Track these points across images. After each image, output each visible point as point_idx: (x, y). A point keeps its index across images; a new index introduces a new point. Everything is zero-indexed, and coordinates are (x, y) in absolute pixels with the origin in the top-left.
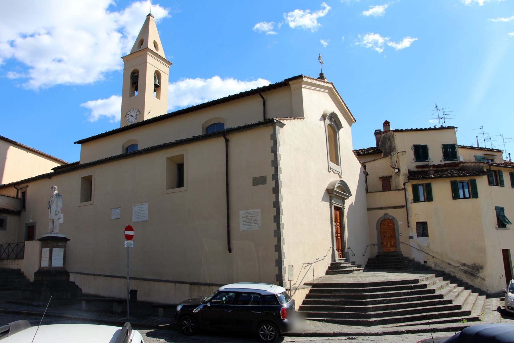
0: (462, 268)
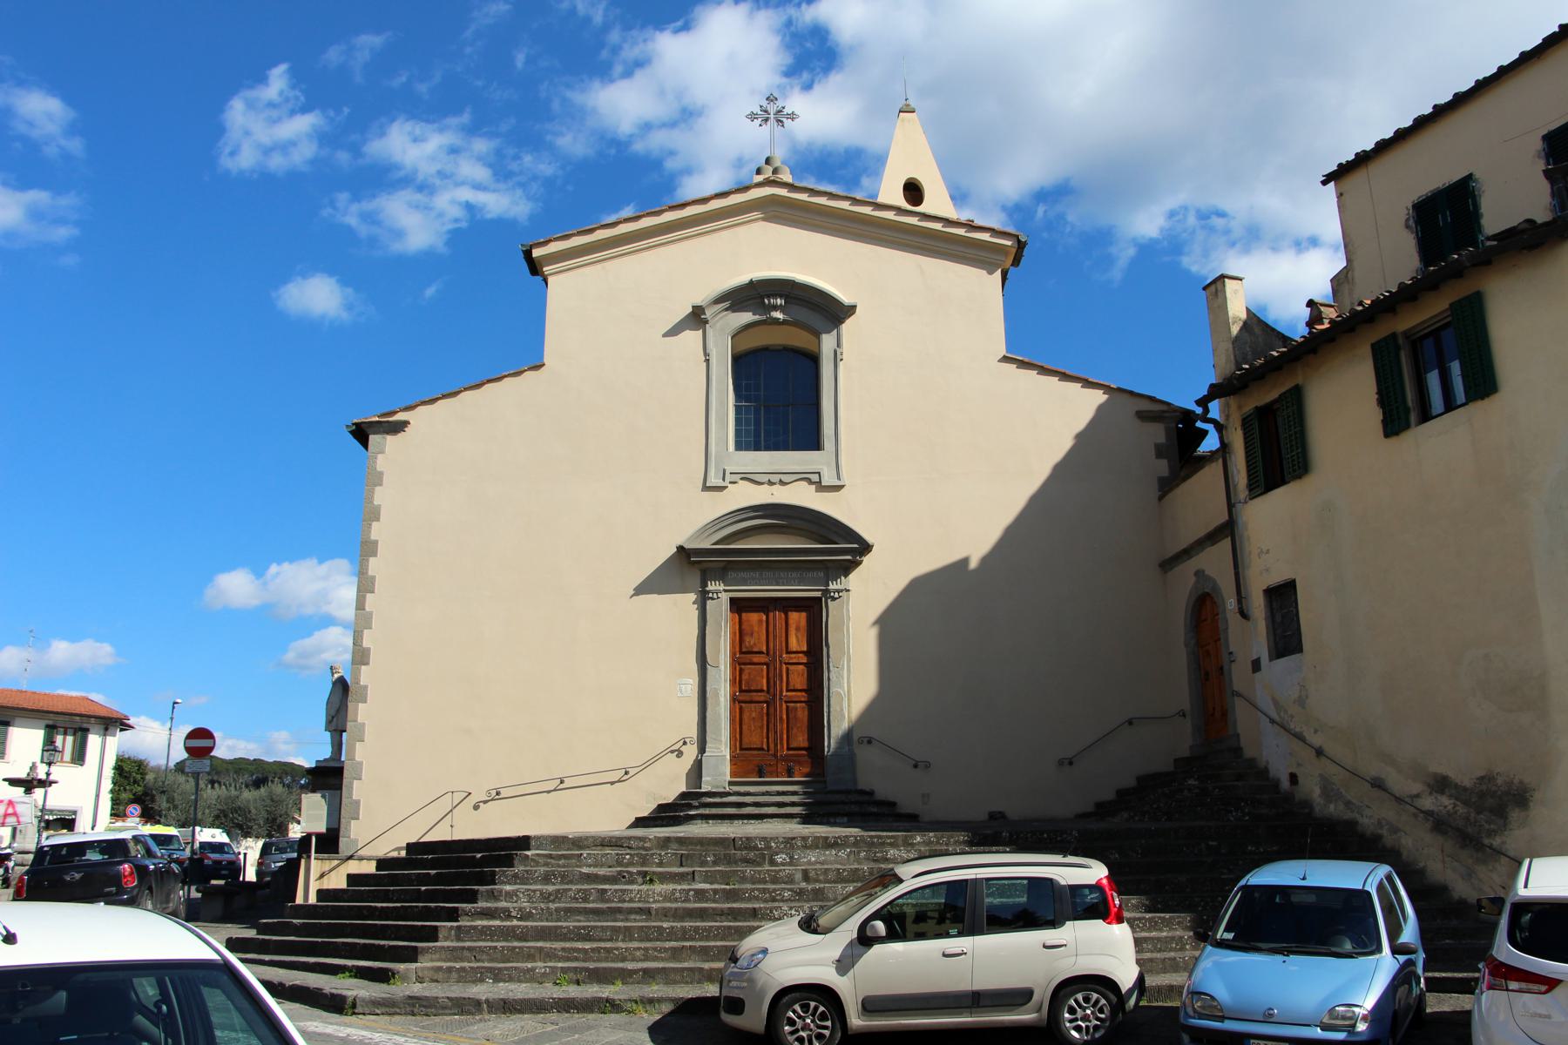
0: (1428, 803)
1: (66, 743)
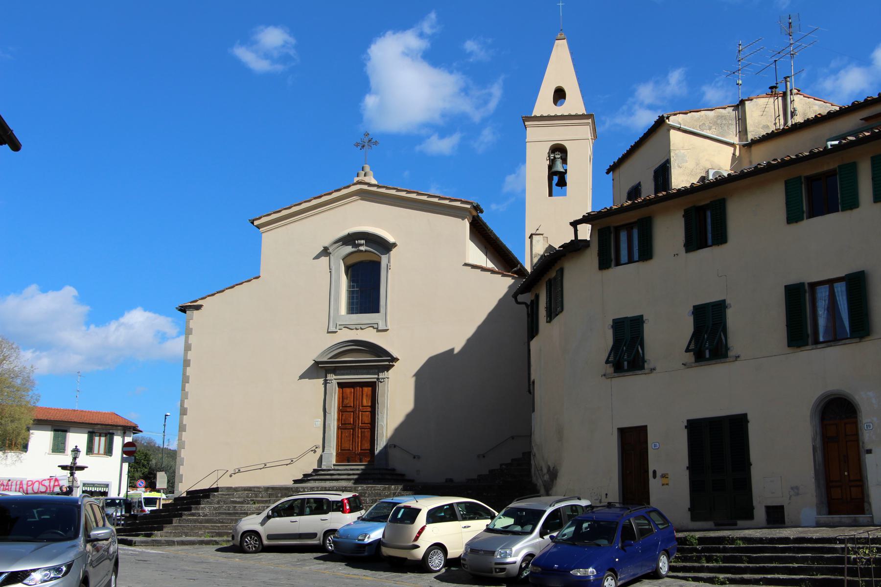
1: (100, 442)
